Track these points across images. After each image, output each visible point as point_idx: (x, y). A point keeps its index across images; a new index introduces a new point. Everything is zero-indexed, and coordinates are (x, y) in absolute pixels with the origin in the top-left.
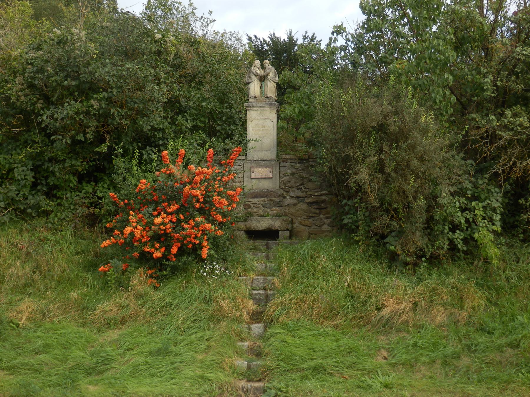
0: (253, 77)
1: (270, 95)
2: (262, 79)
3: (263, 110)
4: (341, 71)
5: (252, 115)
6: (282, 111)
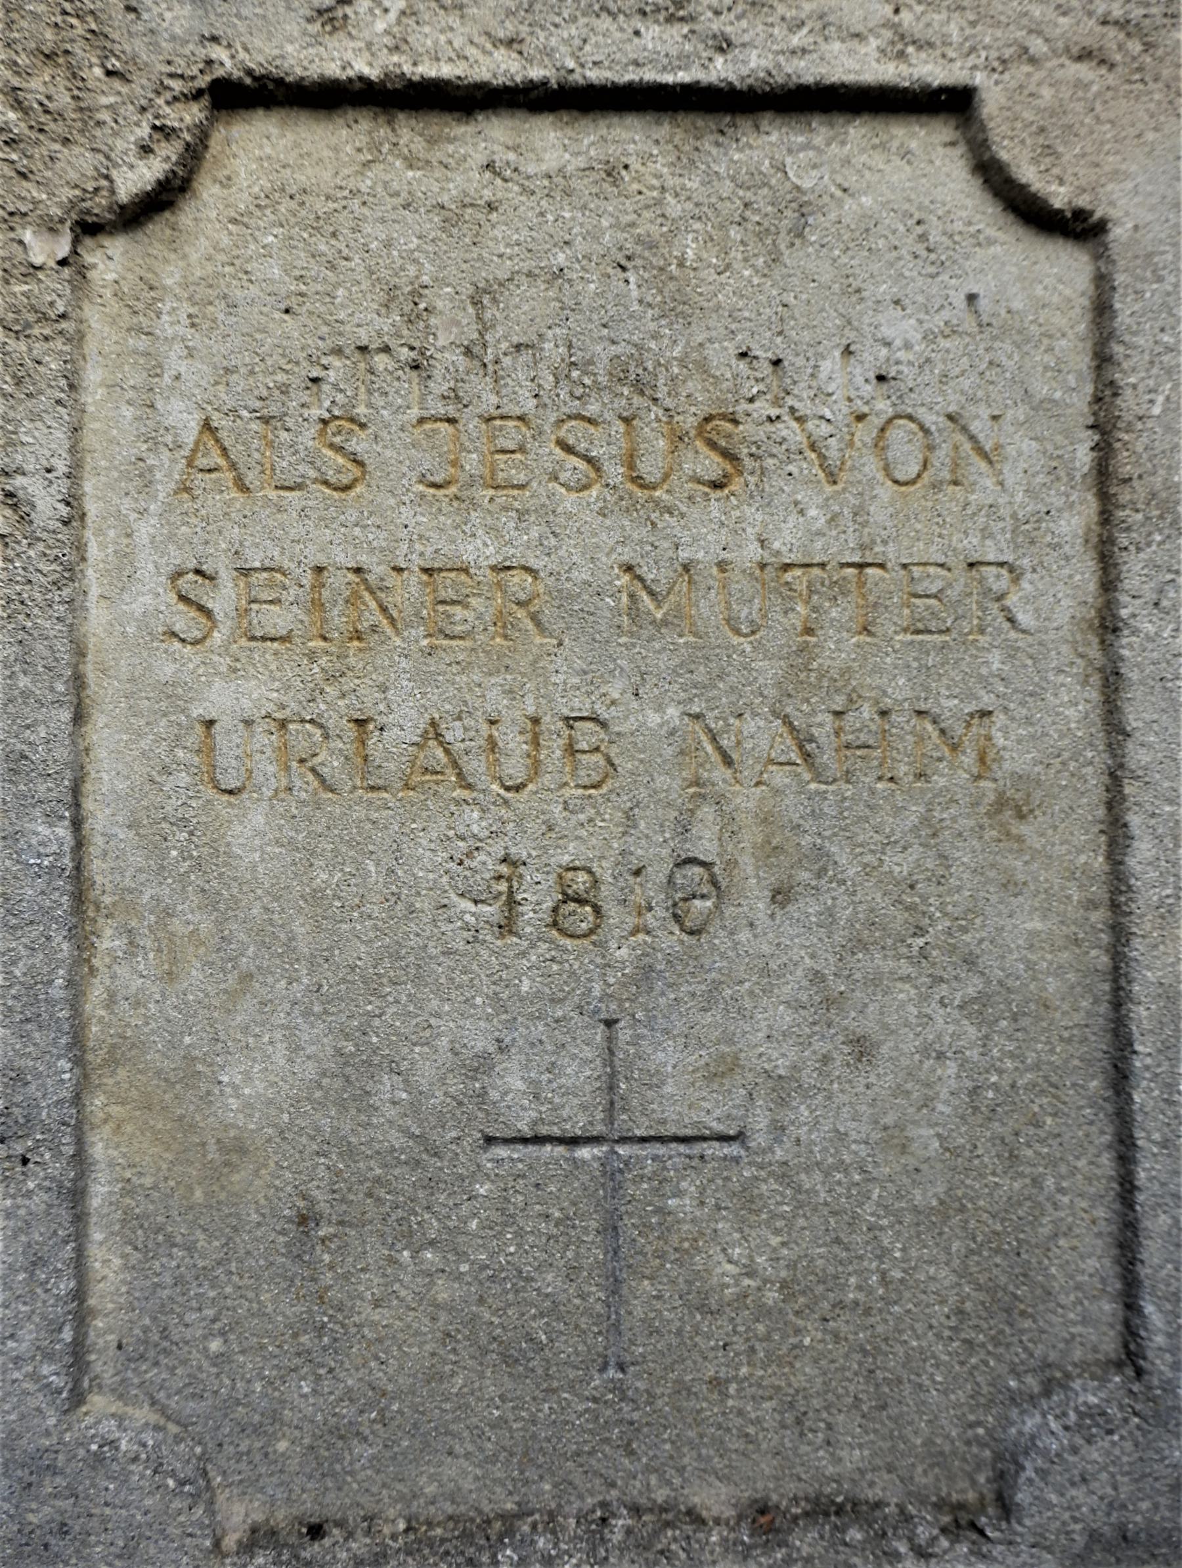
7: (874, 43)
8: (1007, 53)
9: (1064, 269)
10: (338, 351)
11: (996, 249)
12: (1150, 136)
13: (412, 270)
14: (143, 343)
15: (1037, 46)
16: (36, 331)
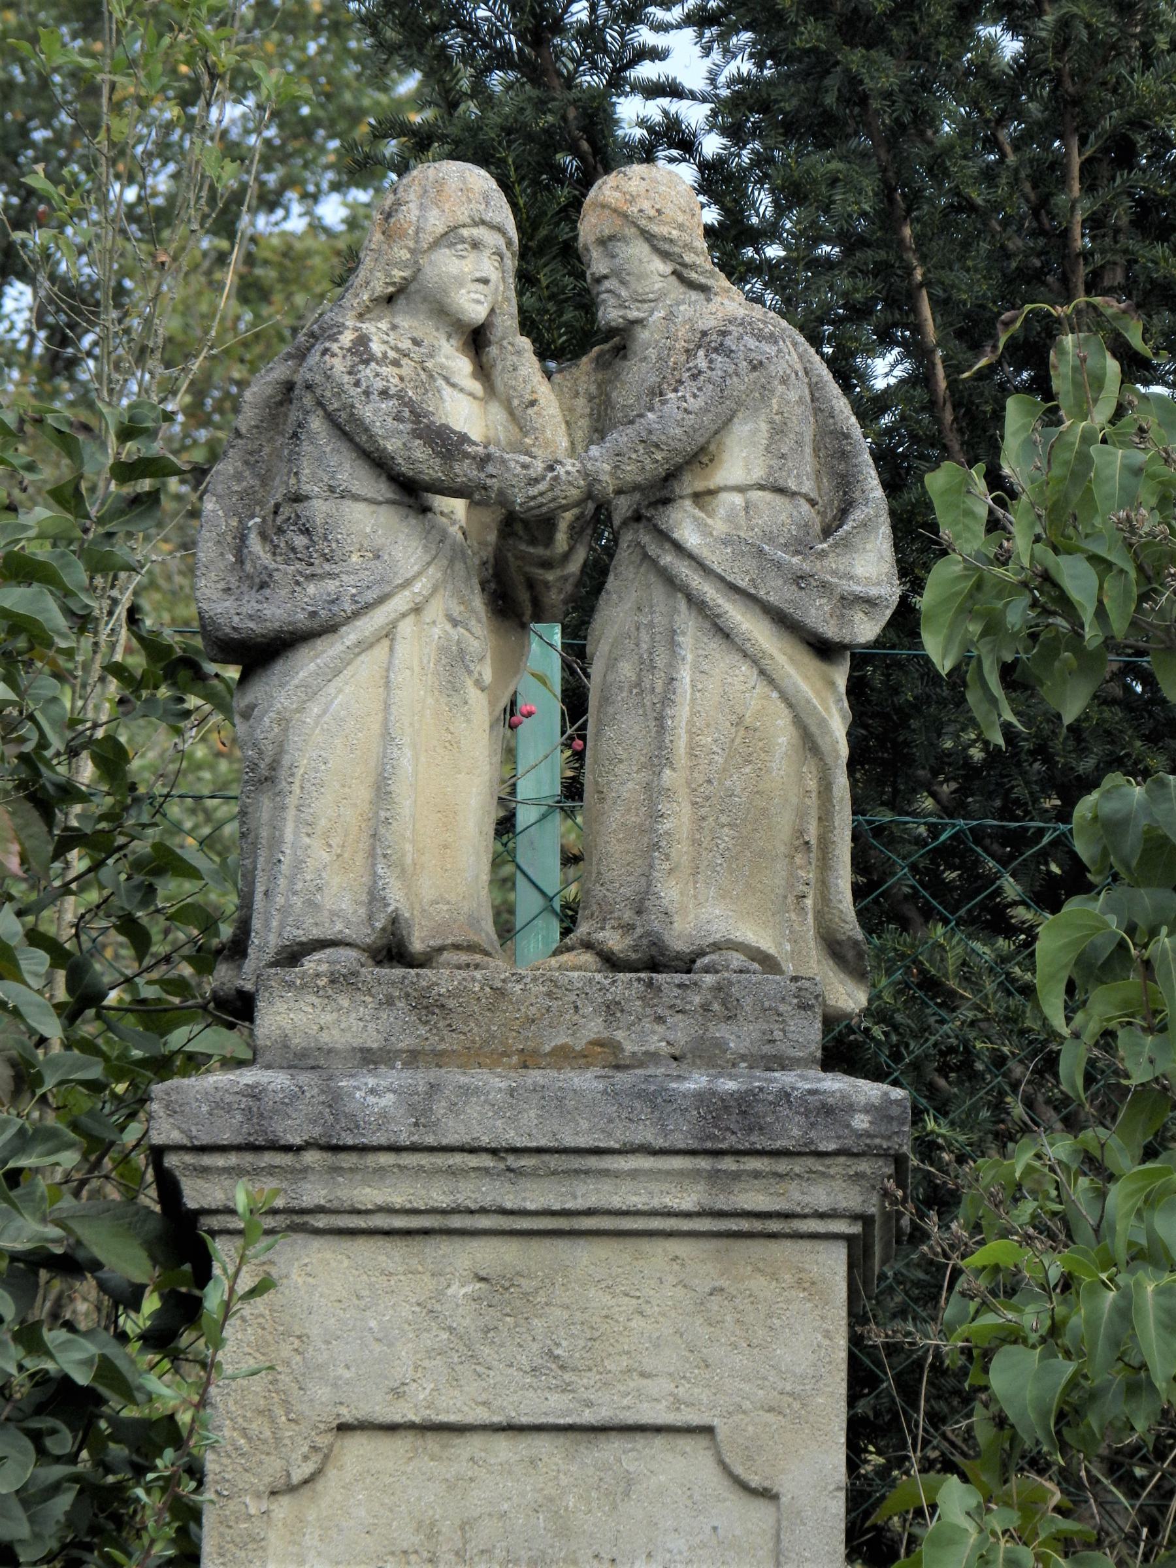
0: (364, 523)
1: (702, 909)
2: (548, 571)
3: (565, 1226)
4: (993, 436)
5: (322, 1319)
6: (1007, 1286)
7: (664, 1403)
8: (731, 1409)
9: (760, 1514)
10: (393, 1553)
11: (728, 1503)
12: (802, 1452)
13: (431, 1512)
14: (295, 1549)
15: (747, 1405)
16: (250, 1546)
